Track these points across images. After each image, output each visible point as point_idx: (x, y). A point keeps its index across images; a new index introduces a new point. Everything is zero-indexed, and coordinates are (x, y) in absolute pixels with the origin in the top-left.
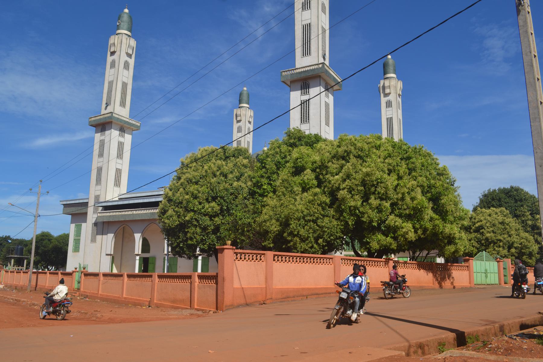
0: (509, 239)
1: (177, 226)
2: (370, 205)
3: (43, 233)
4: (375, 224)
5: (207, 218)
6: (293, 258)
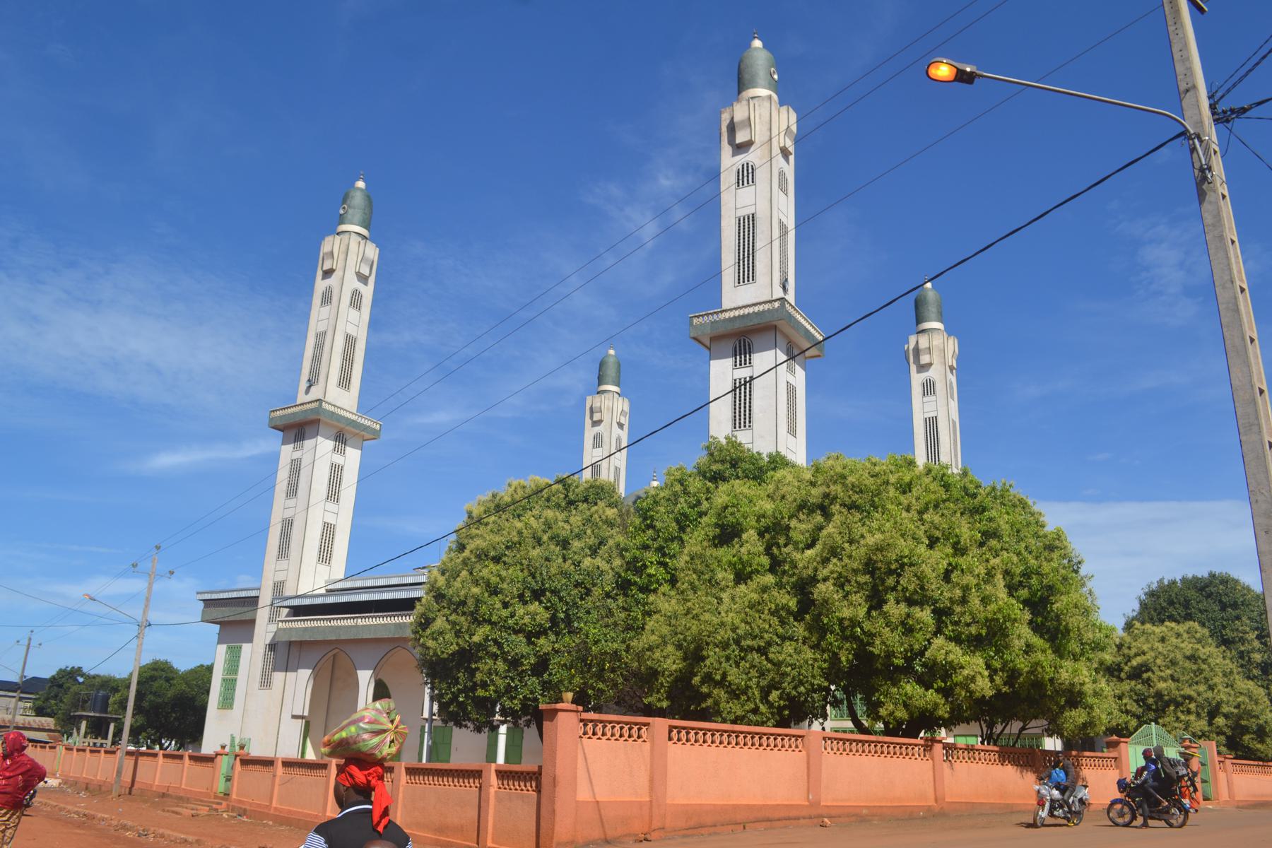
0: (1209, 694)
1: (453, 654)
2: (885, 616)
3: (156, 663)
4: (899, 662)
5: (521, 637)
6: (713, 735)
